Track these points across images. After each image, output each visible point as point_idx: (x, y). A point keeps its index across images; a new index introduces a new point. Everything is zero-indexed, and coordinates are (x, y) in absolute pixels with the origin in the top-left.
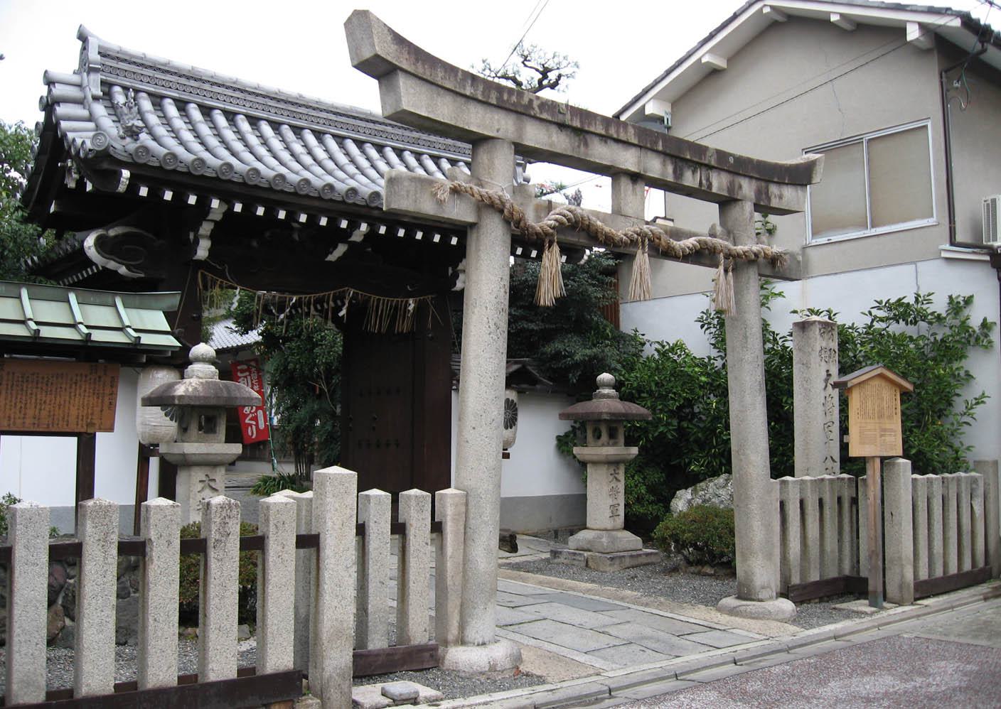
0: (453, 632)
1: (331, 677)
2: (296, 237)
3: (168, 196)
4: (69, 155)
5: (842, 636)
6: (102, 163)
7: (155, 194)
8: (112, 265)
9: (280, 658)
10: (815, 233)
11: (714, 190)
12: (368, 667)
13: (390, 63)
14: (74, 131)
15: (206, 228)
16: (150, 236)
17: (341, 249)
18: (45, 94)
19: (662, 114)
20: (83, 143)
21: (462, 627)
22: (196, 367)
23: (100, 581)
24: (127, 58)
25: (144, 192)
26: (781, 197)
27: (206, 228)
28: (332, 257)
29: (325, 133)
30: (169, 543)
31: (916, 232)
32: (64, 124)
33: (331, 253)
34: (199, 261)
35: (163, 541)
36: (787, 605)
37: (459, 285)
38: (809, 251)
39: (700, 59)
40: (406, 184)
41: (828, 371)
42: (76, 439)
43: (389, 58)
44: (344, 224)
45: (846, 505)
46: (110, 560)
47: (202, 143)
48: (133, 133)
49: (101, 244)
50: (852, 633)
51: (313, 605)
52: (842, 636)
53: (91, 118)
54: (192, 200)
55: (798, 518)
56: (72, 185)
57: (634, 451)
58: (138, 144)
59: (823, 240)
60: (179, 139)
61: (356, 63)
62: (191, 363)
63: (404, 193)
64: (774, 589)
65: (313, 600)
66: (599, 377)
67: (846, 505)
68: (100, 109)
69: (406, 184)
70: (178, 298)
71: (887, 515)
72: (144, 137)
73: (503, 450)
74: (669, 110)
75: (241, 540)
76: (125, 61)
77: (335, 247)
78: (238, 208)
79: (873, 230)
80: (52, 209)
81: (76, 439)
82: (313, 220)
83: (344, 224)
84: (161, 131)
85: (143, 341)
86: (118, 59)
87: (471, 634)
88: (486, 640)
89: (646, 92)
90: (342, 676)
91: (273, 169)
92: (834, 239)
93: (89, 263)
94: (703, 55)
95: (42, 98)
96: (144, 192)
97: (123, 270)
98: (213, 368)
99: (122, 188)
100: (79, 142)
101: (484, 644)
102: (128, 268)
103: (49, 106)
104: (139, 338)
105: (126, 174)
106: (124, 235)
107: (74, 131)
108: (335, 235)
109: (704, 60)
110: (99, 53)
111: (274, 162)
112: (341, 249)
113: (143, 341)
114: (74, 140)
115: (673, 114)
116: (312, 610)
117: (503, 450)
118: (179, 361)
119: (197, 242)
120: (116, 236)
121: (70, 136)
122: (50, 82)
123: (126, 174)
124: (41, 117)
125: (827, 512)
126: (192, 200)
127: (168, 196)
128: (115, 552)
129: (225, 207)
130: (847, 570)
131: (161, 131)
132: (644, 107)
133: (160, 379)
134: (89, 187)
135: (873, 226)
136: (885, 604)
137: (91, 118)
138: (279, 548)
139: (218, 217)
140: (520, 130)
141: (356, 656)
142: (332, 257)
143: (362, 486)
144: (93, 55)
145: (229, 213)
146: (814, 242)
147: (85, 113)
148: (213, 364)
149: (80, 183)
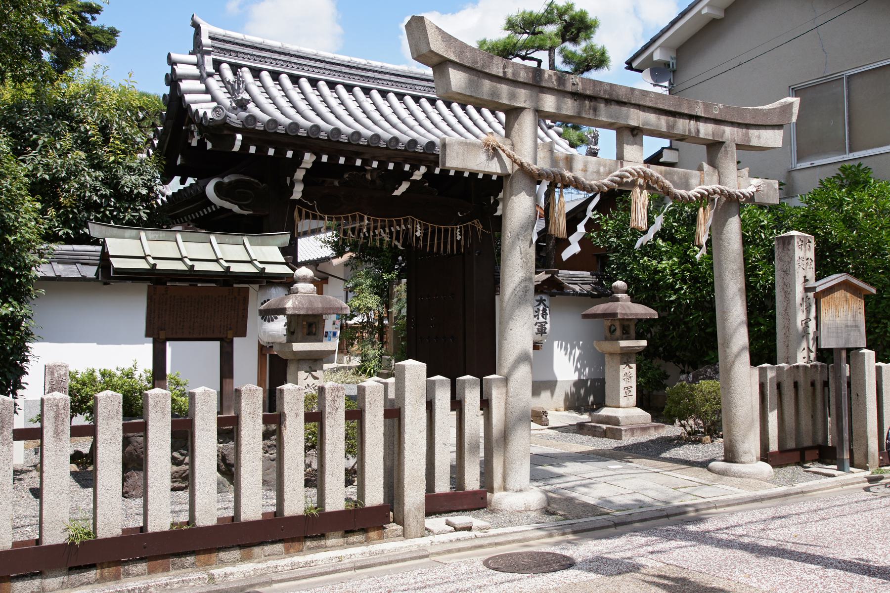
0: (497, 481)
1: (410, 510)
2: (369, 177)
3: (271, 152)
4: (191, 121)
5: (809, 492)
6: (220, 130)
7: (261, 150)
8: (227, 205)
9: (375, 496)
10: (800, 159)
11: (702, 136)
12: (436, 505)
13: (441, 56)
14: (195, 102)
15: (300, 174)
16: (256, 181)
17: (405, 186)
18: (169, 72)
19: (668, 59)
20: (205, 113)
21: (504, 479)
22: (300, 286)
23: (251, 441)
24: (232, 40)
25: (253, 150)
26: (759, 137)
27: (300, 174)
28: (397, 193)
29: (389, 92)
30: (297, 415)
31: (883, 157)
32: (188, 97)
33: (397, 189)
34: (295, 200)
35: (293, 413)
36: (766, 467)
37: (498, 213)
38: (795, 174)
39: (700, 11)
40: (456, 147)
41: (805, 277)
42: (218, 343)
43: (440, 53)
44: (407, 168)
45: (819, 387)
46: (257, 427)
47: (294, 107)
48: (242, 105)
49: (218, 189)
50: (819, 490)
51: (396, 459)
52: (809, 492)
53: (208, 91)
54: (290, 154)
55: (775, 398)
56: (194, 143)
57: (644, 343)
58: (244, 114)
59: (807, 164)
60: (276, 104)
61: (415, 56)
62: (296, 282)
63: (454, 155)
64: (754, 454)
65: (396, 455)
66: (614, 284)
67: (819, 387)
68: (214, 83)
69: (456, 147)
70: (289, 236)
71: (853, 396)
72: (251, 106)
73: (539, 349)
74: (674, 55)
75: (346, 412)
76: (229, 42)
77: (400, 185)
78: (325, 158)
79: (851, 155)
80: (179, 162)
81: (218, 343)
82: (383, 164)
83: (407, 168)
84: (262, 98)
85: (266, 271)
86: (224, 41)
87: (511, 483)
88: (522, 488)
89: (653, 41)
90: (418, 509)
91: (349, 126)
92: (817, 162)
93: (210, 203)
94: (703, 8)
95: (167, 75)
96: (253, 150)
97: (236, 209)
98: (312, 286)
99: (237, 148)
100: (201, 113)
101: (521, 491)
102: (240, 207)
103: (173, 80)
104: (264, 269)
105: (239, 137)
106: (237, 181)
107: (195, 102)
108: (400, 176)
109: (704, 12)
110: (210, 37)
111: (350, 120)
112: (405, 186)
113: (266, 271)
114: (197, 110)
115: (677, 58)
116: (396, 463)
117: (539, 349)
118: (287, 283)
119: (292, 185)
120: (230, 183)
121: (194, 107)
122: (172, 63)
123: (239, 137)
124: (167, 90)
125: (801, 392)
126: (290, 154)
127: (271, 152)
128: (261, 421)
129: (314, 158)
130: (820, 440)
131: (262, 98)
132: (652, 53)
133: (275, 295)
134: (209, 146)
135: (851, 151)
136: (852, 469)
137: (208, 91)
138: (373, 418)
139: (309, 166)
140: (538, 100)
141: (428, 498)
142: (397, 193)
143: (430, 374)
144: (205, 40)
145: (317, 163)
146: (799, 166)
147: (203, 87)
148: (311, 282)
149: (202, 143)
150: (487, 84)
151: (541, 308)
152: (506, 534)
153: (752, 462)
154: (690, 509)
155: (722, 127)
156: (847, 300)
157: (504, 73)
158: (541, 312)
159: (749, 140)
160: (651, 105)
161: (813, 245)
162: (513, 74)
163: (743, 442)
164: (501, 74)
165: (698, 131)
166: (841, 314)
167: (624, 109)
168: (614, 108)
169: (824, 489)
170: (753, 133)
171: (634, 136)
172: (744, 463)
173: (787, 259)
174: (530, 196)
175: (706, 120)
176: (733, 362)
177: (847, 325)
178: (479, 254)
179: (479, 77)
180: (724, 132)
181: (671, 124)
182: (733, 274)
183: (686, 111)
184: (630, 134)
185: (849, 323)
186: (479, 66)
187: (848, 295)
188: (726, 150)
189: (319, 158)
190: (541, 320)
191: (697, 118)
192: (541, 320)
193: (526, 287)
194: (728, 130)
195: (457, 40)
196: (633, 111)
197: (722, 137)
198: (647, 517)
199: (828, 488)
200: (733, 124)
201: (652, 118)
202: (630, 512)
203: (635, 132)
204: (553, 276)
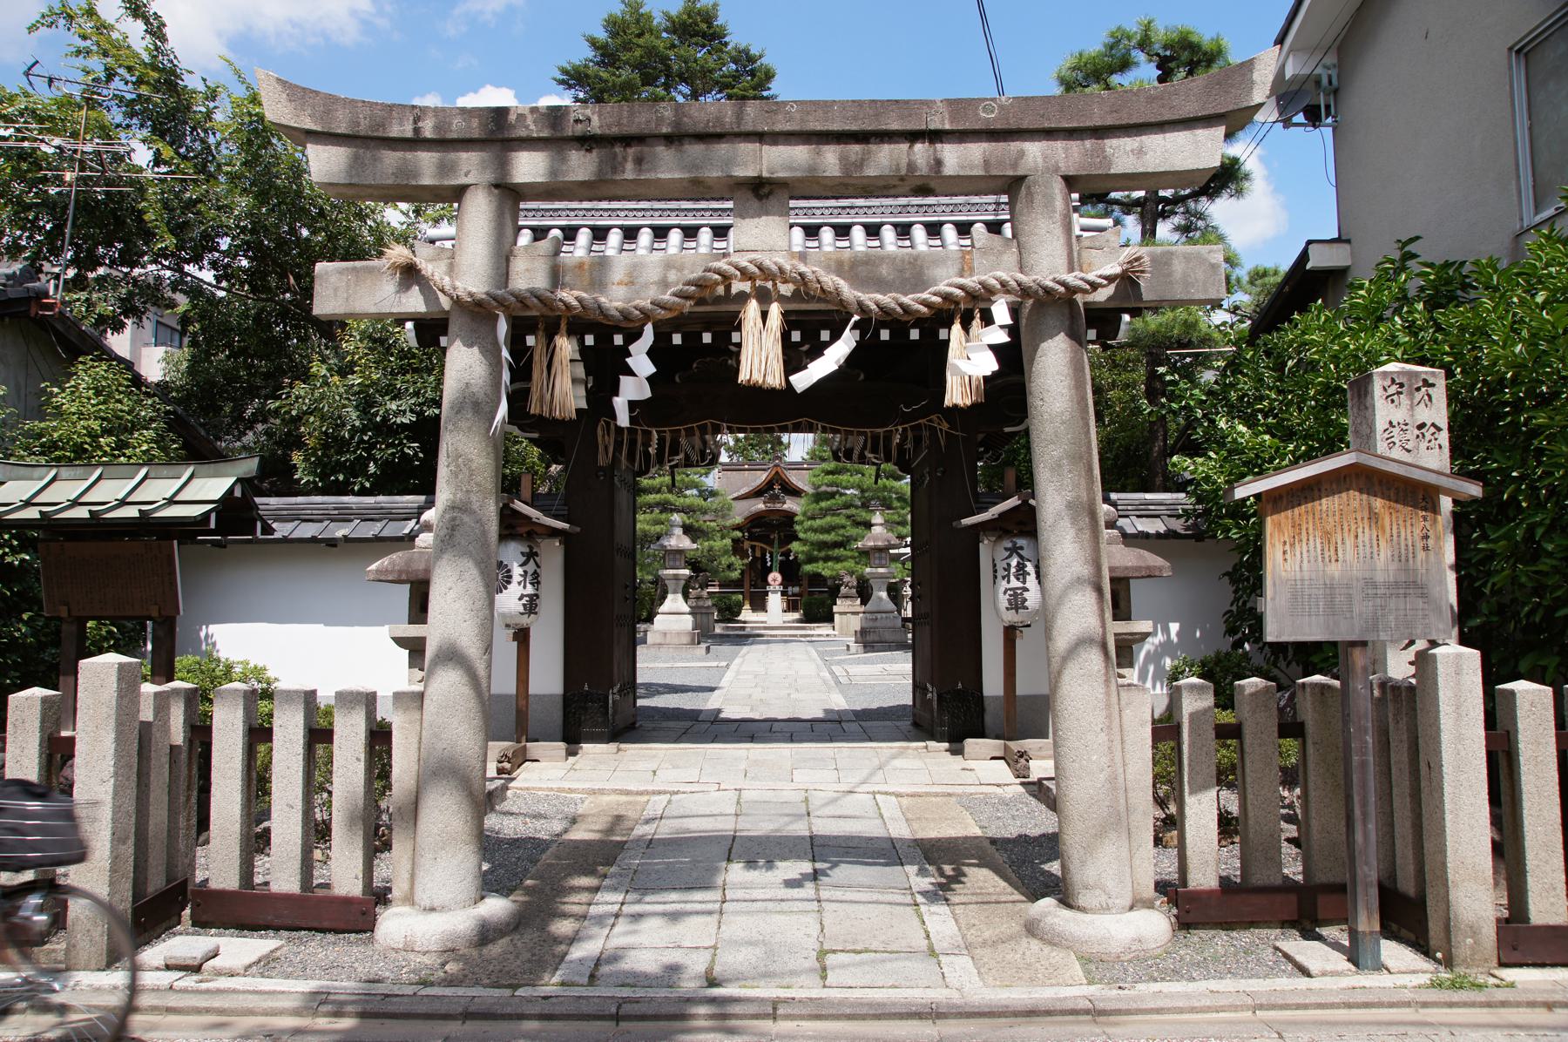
1: (77, 918)
52: (1128, 1012)
69: (333, 279)
101: (433, 909)
138: (18, 751)
140: (503, 165)
150: (391, 158)
151: (1014, 562)
152: (235, 991)
153: (1105, 909)
154: (702, 1010)
155: (1015, 146)
156: (1373, 517)
157: (417, 130)
158: (1013, 570)
159: (1107, 161)
160: (788, 127)
161: (1439, 393)
162: (437, 128)
163: (1083, 863)
164: (409, 134)
165: (939, 163)
166: (1348, 552)
167: (723, 148)
168: (695, 150)
169: (1181, 1011)
170: (1114, 145)
171: (760, 197)
172: (1083, 910)
173: (1365, 430)
174: (470, 346)
175: (962, 136)
176: (1059, 673)
177: (1370, 583)
178: (943, 473)
179: (368, 148)
180: (1022, 154)
181: (853, 158)
182: (1052, 469)
183: (895, 126)
184: (750, 195)
185: (1380, 577)
186: (363, 129)
187: (1378, 503)
188: (1030, 194)
189: (581, 342)
190: (1015, 583)
191: (935, 136)
192: (1015, 583)
193: (454, 519)
194: (1034, 151)
195: (317, 93)
196: (746, 148)
197: (1015, 165)
198: (558, 1010)
199: (1193, 1010)
200: (1049, 134)
201: (798, 154)
202: (640, 993)
203: (766, 190)
204: (1025, 502)
